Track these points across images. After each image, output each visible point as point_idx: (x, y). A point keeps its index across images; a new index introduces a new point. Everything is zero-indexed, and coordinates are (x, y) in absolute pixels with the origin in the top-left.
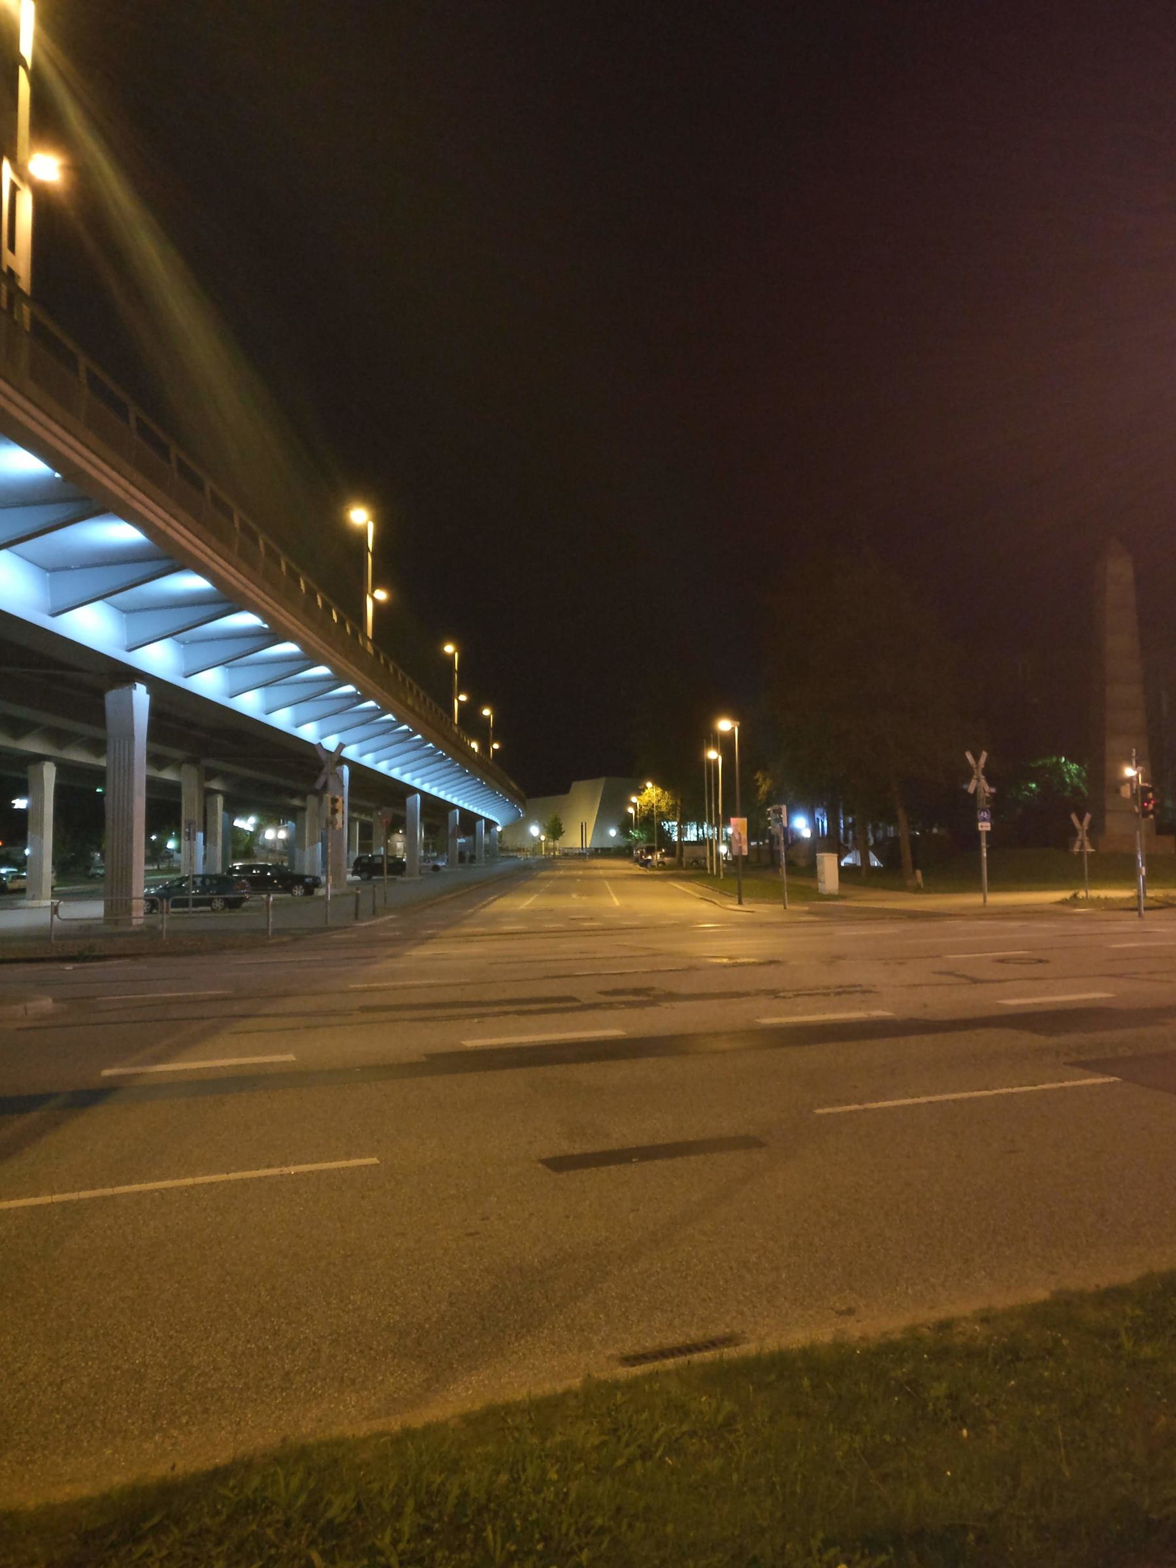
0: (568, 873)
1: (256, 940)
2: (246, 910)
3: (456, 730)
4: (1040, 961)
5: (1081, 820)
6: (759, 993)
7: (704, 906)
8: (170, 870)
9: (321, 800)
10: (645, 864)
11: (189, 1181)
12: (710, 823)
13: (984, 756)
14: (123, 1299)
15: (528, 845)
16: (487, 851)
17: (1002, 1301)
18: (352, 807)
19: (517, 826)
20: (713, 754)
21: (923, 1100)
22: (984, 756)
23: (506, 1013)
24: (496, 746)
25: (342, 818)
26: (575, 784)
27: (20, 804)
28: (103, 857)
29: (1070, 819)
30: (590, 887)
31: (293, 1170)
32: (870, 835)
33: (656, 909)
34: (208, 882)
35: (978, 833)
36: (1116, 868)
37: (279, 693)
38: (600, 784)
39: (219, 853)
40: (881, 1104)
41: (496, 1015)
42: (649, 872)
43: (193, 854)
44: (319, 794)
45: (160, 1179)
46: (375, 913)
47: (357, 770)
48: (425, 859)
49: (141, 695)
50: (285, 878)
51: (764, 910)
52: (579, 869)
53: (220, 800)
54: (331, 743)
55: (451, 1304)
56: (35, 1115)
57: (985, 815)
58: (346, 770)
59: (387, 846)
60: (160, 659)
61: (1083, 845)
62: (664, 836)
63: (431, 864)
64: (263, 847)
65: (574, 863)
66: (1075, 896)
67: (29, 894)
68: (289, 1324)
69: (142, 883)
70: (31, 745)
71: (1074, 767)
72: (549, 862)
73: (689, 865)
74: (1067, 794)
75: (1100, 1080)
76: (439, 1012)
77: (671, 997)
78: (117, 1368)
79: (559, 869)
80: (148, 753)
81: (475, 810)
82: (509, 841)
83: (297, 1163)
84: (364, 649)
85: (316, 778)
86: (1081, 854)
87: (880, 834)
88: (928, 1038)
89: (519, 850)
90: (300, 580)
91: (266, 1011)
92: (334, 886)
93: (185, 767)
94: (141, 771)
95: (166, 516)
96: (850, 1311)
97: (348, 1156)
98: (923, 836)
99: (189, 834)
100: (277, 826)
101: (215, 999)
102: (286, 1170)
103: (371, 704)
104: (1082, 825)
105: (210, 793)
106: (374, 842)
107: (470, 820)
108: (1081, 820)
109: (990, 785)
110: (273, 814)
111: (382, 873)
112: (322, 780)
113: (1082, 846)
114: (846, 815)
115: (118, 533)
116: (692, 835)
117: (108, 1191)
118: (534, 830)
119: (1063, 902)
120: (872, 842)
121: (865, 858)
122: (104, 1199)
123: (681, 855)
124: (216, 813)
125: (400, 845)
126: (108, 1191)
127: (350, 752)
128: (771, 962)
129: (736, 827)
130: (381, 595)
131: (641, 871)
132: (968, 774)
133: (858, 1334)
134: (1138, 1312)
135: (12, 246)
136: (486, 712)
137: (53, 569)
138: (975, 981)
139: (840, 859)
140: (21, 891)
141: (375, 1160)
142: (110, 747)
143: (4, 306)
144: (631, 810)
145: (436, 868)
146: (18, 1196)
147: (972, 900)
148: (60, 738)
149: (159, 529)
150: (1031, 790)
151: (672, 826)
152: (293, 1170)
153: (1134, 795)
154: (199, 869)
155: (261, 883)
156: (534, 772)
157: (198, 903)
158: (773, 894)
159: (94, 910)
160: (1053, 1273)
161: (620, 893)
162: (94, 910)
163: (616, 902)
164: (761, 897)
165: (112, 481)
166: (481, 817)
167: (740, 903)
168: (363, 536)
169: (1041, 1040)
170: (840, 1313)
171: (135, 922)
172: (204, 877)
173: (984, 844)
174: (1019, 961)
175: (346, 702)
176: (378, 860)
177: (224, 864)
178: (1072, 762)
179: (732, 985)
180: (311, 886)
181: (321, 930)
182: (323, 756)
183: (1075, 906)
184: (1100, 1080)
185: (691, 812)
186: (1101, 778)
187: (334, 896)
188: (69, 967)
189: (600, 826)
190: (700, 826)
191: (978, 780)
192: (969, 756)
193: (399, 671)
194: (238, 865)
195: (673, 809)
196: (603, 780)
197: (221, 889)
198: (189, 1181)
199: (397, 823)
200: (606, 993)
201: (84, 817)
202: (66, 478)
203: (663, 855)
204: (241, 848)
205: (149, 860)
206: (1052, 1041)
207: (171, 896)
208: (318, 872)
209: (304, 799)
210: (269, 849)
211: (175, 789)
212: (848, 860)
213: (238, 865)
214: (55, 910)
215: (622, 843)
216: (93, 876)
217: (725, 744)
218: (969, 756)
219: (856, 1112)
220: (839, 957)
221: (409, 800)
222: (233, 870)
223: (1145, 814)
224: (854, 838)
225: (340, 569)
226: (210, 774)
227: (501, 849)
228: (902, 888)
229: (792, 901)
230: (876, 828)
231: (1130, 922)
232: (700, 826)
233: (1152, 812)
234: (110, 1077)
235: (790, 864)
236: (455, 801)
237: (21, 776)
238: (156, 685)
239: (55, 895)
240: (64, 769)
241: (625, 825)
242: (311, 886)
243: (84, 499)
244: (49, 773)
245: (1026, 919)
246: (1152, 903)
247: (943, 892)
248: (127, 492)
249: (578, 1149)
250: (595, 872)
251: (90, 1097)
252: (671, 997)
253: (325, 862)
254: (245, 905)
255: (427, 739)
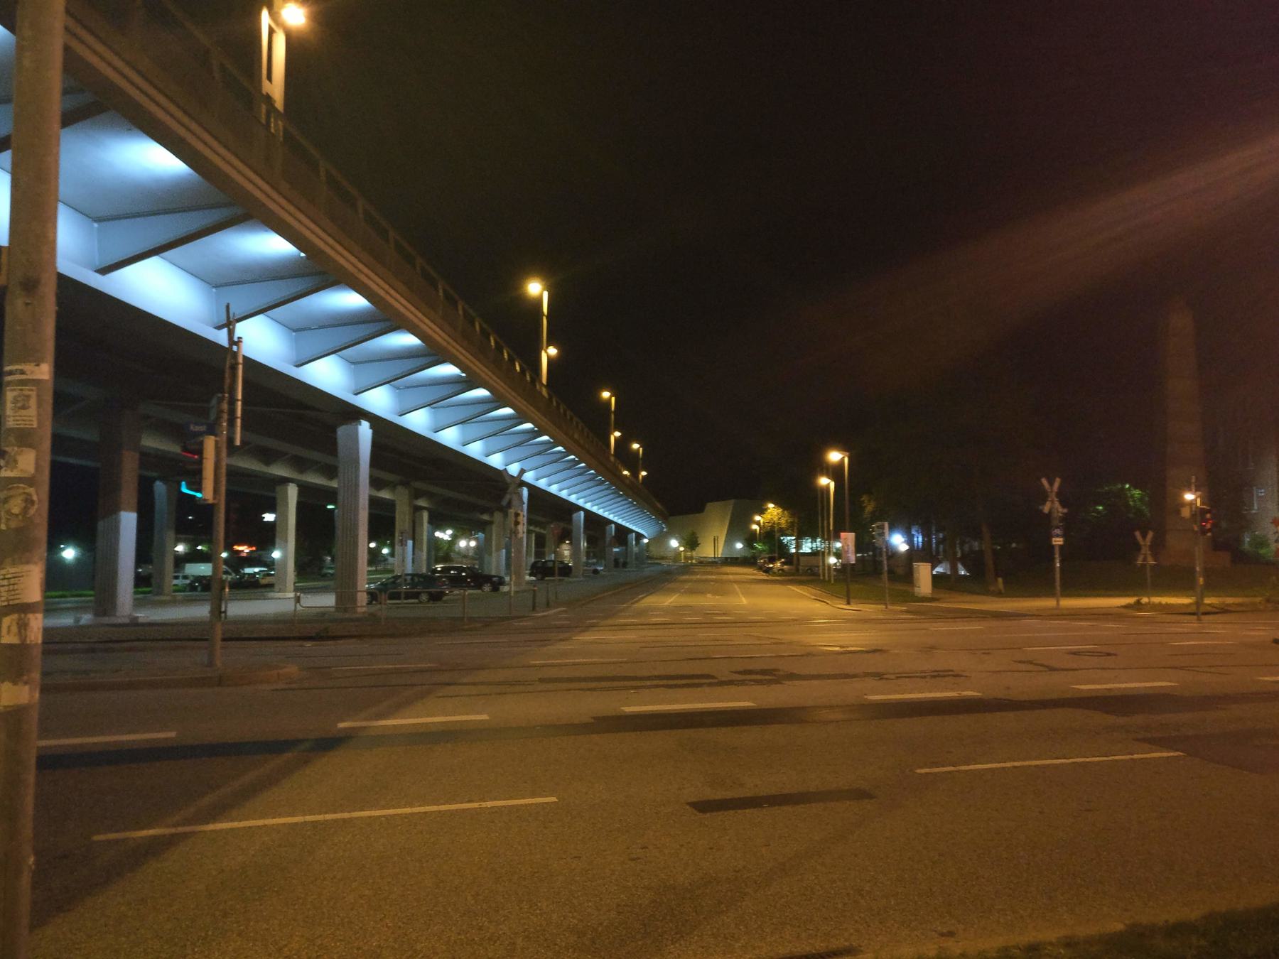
0: (705, 577)
1: (455, 626)
2: (446, 602)
3: (612, 459)
4: (1109, 654)
5: (1144, 537)
6: (867, 675)
7: (818, 605)
8: (386, 571)
9: (506, 515)
10: (767, 571)
11: (408, 810)
12: (823, 538)
13: (1057, 482)
14: (361, 897)
15: (670, 555)
16: (637, 559)
17: (1082, 931)
18: (530, 522)
19: (660, 539)
20: (824, 481)
21: (1008, 765)
22: (1057, 482)
23: (657, 686)
24: (644, 473)
25: (522, 529)
26: (709, 506)
27: (269, 517)
28: (333, 560)
29: (1135, 537)
30: (721, 588)
31: (489, 804)
32: (958, 549)
33: (775, 606)
34: (416, 579)
35: (1053, 547)
36: (1177, 579)
37: (473, 429)
38: (730, 504)
39: (425, 557)
40: (971, 767)
41: (649, 687)
42: (771, 578)
43: (405, 558)
44: (504, 510)
45: (383, 808)
46: (548, 605)
47: (535, 492)
48: (587, 564)
49: (365, 429)
50: (477, 578)
51: (869, 609)
52: (712, 574)
53: (425, 515)
54: (514, 469)
55: (619, 913)
56: (289, 755)
57: (1058, 531)
58: (525, 491)
59: (555, 552)
60: (379, 401)
61: (1146, 559)
62: (783, 549)
63: (592, 568)
64: (459, 553)
65: (709, 569)
66: (1138, 602)
67: (277, 588)
68: (490, 922)
69: (365, 582)
70: (279, 470)
71: (1137, 493)
72: (687, 569)
73: (805, 572)
74: (1131, 516)
75: (1165, 755)
76: (603, 684)
77: (792, 677)
78: (358, 949)
79: (696, 574)
80: (371, 477)
81: (627, 525)
82: (654, 551)
83: (492, 800)
84: (540, 393)
85: (501, 497)
86: (1144, 566)
87: (966, 548)
88: (1011, 715)
89: (663, 558)
90: (488, 338)
91: (465, 680)
92: (516, 584)
93: (400, 488)
94: (365, 492)
95: (387, 287)
96: (951, 934)
97: (534, 795)
98: (1003, 553)
99: (401, 541)
100: (469, 538)
101: (422, 671)
102: (484, 805)
103: (546, 438)
104: (1145, 541)
105: (418, 509)
106: (547, 550)
107: (623, 532)
108: (1144, 537)
109: (1064, 507)
110: (465, 528)
111: (553, 575)
112: (508, 497)
113: (1145, 560)
114: (938, 531)
115: (349, 300)
116: (807, 547)
117: (346, 815)
118: (674, 543)
119: (1127, 607)
120: (959, 555)
121: (954, 569)
122: (344, 820)
123: (798, 564)
124: (422, 525)
125: (567, 553)
126: (346, 815)
127: (529, 477)
128: (874, 651)
129: (849, 538)
130: (553, 351)
131: (764, 576)
132: (1044, 497)
133: (959, 951)
134: (1203, 942)
135: (269, 78)
136: (636, 446)
137: (297, 329)
138: (1052, 669)
139: (933, 568)
140: (270, 586)
141: (554, 799)
142: (341, 469)
143: (263, 121)
144: (755, 527)
145: (596, 572)
146: (280, 816)
147: (1049, 603)
148: (300, 464)
149: (378, 295)
150: (1098, 512)
151: (789, 540)
152: (489, 804)
153: (1193, 516)
154: (409, 569)
155: (457, 581)
156: (674, 499)
157: (408, 596)
158: (879, 598)
159: (327, 601)
160: (1126, 910)
161: (746, 594)
162: (327, 601)
163: (744, 601)
164: (866, 599)
165: (346, 260)
166: (632, 531)
167: (848, 603)
168: (539, 301)
169: (1111, 719)
170: (942, 935)
171: (359, 610)
172: (413, 575)
173: (1057, 556)
174: (1092, 654)
175: (527, 436)
176: (550, 565)
177: (429, 565)
178: (1136, 488)
179: (842, 668)
180: (497, 583)
181: (507, 618)
182: (508, 480)
183: (1140, 610)
184: (1165, 755)
185: (806, 528)
186: (1163, 501)
187: (516, 592)
188: (308, 644)
189: (730, 541)
190: (814, 540)
191: (1052, 502)
192: (1044, 481)
193: (566, 412)
194: (439, 567)
195: (791, 525)
196: (732, 501)
197: (426, 586)
198: (408, 810)
199: (566, 535)
200: (739, 673)
201: (318, 532)
202: (308, 258)
203: (783, 564)
204: (441, 554)
205: (370, 563)
206: (1122, 720)
207: (388, 590)
208: (502, 574)
209: (492, 514)
210: (464, 555)
211: (391, 505)
212: (939, 569)
213: (439, 567)
214: (298, 600)
215: (748, 554)
216: (325, 575)
217: (835, 472)
218: (1044, 481)
219: (950, 772)
220: (933, 648)
221: (575, 515)
222: (435, 571)
223: (1204, 532)
224: (945, 551)
225: (518, 329)
226: (417, 494)
227: (649, 557)
228: (987, 593)
229: (893, 604)
230: (962, 544)
231: (1190, 624)
232: (814, 540)
233: (1210, 530)
234: (345, 729)
235: (890, 572)
236: (611, 517)
237: (271, 494)
238: (375, 421)
239: (296, 589)
240: (304, 489)
241: (750, 539)
242: (497, 583)
243: (323, 273)
244: (292, 492)
245: (1096, 620)
246: (1209, 609)
247: (1023, 596)
248: (355, 267)
249: (720, 794)
250: (725, 577)
251: (329, 743)
252: (792, 677)
253: (508, 565)
254: (445, 598)
255: (589, 467)
